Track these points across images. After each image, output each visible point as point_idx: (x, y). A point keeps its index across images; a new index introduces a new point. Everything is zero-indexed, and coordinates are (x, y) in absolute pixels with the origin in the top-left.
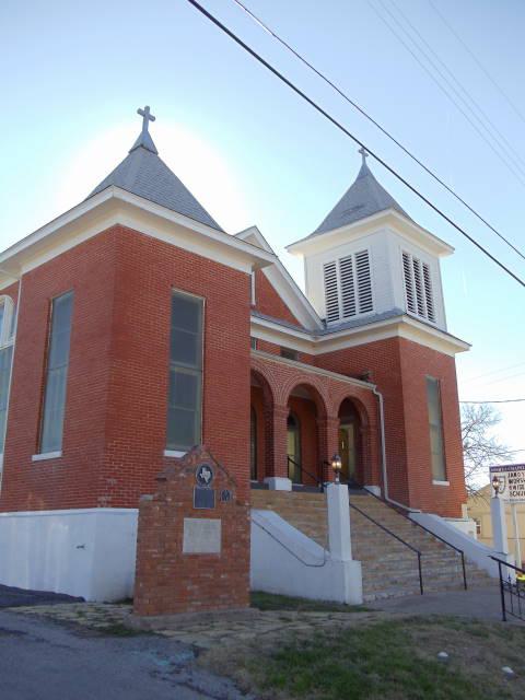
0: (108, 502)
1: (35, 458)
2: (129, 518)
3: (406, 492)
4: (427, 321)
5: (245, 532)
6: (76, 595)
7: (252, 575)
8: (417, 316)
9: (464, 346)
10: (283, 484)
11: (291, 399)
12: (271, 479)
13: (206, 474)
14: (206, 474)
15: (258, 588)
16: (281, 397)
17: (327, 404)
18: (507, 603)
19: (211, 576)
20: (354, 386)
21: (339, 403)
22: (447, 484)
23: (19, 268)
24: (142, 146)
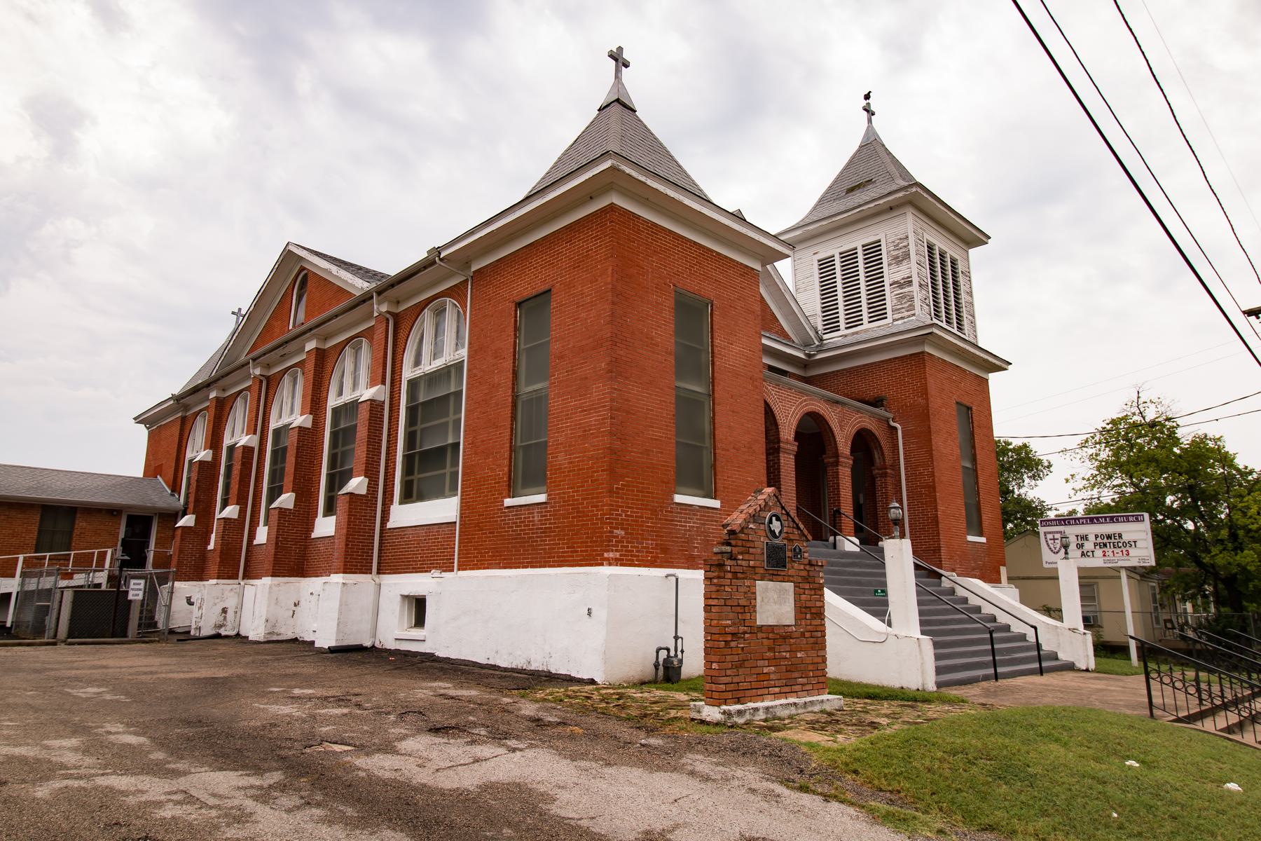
0: (616, 559)
1: (508, 502)
3: (937, 550)
4: (955, 331)
6: (585, 677)
8: (944, 325)
9: (999, 365)
11: (797, 434)
13: (776, 526)
14: (776, 526)
19: (788, 656)
20: (864, 419)
21: (851, 438)
22: (983, 540)
23: (470, 267)
24: (618, 100)
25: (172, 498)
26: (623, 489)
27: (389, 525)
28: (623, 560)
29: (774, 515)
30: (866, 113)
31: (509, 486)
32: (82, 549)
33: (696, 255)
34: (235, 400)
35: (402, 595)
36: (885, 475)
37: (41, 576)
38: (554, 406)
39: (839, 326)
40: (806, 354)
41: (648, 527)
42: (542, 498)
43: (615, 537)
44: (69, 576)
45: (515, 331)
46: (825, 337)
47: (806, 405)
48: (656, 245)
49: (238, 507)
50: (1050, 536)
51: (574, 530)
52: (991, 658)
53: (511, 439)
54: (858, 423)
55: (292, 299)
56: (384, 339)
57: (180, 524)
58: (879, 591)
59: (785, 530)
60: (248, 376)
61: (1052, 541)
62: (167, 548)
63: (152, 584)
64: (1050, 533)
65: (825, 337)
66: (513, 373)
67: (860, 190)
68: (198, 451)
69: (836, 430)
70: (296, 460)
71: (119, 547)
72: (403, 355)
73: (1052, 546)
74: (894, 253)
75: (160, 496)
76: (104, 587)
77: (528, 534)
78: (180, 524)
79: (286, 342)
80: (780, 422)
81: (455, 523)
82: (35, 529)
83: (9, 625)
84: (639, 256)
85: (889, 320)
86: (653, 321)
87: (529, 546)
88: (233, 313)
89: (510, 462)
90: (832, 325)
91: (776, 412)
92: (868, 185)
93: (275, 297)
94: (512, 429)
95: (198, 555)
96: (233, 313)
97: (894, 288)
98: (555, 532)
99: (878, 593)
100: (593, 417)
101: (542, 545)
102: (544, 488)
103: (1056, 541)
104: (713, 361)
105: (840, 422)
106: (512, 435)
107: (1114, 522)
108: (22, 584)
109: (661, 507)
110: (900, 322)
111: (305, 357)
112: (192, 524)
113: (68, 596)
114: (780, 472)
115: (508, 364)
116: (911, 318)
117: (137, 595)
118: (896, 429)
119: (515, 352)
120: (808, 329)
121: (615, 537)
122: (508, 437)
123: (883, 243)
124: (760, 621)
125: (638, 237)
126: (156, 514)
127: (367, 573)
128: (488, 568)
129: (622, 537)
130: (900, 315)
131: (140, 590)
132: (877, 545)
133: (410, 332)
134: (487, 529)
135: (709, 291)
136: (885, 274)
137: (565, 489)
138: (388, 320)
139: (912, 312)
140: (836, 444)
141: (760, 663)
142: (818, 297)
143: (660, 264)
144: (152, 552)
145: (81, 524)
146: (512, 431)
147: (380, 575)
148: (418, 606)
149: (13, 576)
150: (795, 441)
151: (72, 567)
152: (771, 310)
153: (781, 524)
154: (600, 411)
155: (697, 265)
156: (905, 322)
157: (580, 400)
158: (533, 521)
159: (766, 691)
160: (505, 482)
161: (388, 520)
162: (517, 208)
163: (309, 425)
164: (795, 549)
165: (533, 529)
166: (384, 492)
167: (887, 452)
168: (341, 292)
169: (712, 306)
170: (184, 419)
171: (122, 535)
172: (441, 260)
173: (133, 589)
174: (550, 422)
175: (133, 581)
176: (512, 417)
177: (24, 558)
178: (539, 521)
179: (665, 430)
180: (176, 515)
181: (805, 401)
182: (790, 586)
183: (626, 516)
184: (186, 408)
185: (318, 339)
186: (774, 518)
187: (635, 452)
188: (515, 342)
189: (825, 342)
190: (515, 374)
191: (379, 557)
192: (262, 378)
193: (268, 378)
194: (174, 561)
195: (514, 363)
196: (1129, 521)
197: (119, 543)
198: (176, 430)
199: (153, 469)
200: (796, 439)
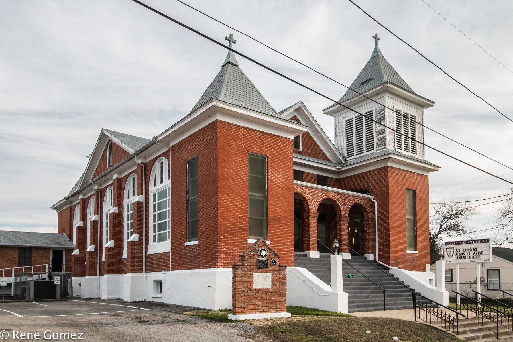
0: (221, 266)
1: (186, 244)
2: (427, 264)
4: (410, 154)
5: (284, 279)
7: (287, 298)
10: (314, 254)
12: (308, 251)
13: (263, 253)
15: (289, 305)
16: (313, 207)
17: (342, 209)
18: (417, 315)
19: (267, 299)
21: (349, 209)
22: (417, 252)
25: (70, 242)
26: (224, 239)
27: (148, 253)
28: (224, 266)
29: (262, 249)
30: (375, 39)
31: (186, 237)
32: (36, 265)
33: (259, 136)
34: (90, 199)
35: (155, 281)
36: (368, 224)
37: (22, 276)
38: (200, 205)
39: (353, 154)
40: (337, 168)
41: (236, 253)
42: (196, 242)
43: (220, 257)
44: (31, 276)
45: (186, 173)
46: (347, 159)
47: (324, 196)
48: (239, 135)
49: (94, 246)
50: (448, 250)
51: (207, 255)
52: (383, 302)
53: (186, 219)
54: (354, 201)
55: (107, 154)
56: (141, 175)
57: (73, 253)
58: (351, 276)
59: (268, 254)
60: (92, 190)
61: (449, 252)
62: (70, 263)
63: (65, 278)
64: (449, 248)
65: (347, 159)
66: (186, 191)
67: (367, 84)
68: (77, 223)
69: (341, 205)
70: (113, 227)
71: (51, 264)
72: (149, 181)
73: (449, 254)
74: (378, 117)
75: (65, 243)
76: (47, 280)
77: (193, 256)
78: (73, 253)
79: (105, 175)
80: (310, 204)
81: (170, 252)
82: (17, 257)
83: (12, 295)
84: (231, 141)
85: (375, 151)
86: (244, 165)
87: (193, 261)
88: (87, 157)
89: (186, 228)
90: (350, 153)
91: (308, 200)
92: (371, 81)
93: (100, 154)
94: (187, 214)
95: (306, 237)
96: (87, 157)
97: (377, 134)
98: (201, 255)
99: (350, 276)
100: (212, 210)
101: (197, 261)
102: (197, 238)
103: (451, 252)
104: (267, 182)
105: (343, 202)
106: (186, 217)
107: (476, 243)
108: (15, 279)
109: (241, 245)
110: (379, 152)
111: (113, 182)
112: (78, 253)
113: (32, 284)
114: (309, 226)
115: (184, 188)
116: (384, 150)
117: (58, 283)
118: (374, 203)
119: (186, 182)
120: (339, 156)
121: (220, 257)
122: (185, 218)
123: (374, 112)
124: (254, 287)
125: (230, 132)
126: (64, 249)
127: (141, 272)
128: (181, 270)
129: (224, 257)
130: (379, 148)
131: (59, 280)
132: (364, 256)
133: (151, 172)
134: (180, 255)
135: (265, 151)
136: (374, 128)
137: (204, 239)
138: (142, 166)
139: (384, 147)
140: (341, 212)
141: (255, 301)
142: (345, 139)
143: (241, 143)
144: (65, 265)
145: (35, 254)
146: (187, 215)
147: (147, 273)
148: (159, 284)
149: (11, 276)
150: (318, 212)
151: (34, 272)
152: (320, 148)
153: (266, 252)
154: (214, 208)
155: (259, 141)
156: (381, 152)
157: (208, 203)
158: (194, 251)
159: (257, 310)
160: (185, 236)
161: (148, 251)
162: (182, 121)
163: (117, 211)
164: (272, 261)
165: (194, 254)
166: (146, 240)
167: (369, 214)
168: (125, 152)
169: (267, 158)
170: (71, 208)
171: (51, 258)
172: (157, 142)
173: (56, 280)
174: (199, 212)
175: (55, 277)
176: (186, 209)
177: (15, 269)
178: (196, 251)
179: (243, 213)
180: (72, 250)
181: (324, 193)
182: (270, 275)
183: (225, 249)
184: (71, 203)
185: (117, 173)
186: (262, 250)
187: (229, 224)
188: (186, 178)
189: (347, 161)
190: (187, 192)
191: (145, 266)
192: (98, 190)
193: (101, 190)
194: (73, 269)
195: (186, 187)
196: (482, 242)
197: (51, 262)
198: (68, 212)
199: (61, 230)
200: (318, 211)
